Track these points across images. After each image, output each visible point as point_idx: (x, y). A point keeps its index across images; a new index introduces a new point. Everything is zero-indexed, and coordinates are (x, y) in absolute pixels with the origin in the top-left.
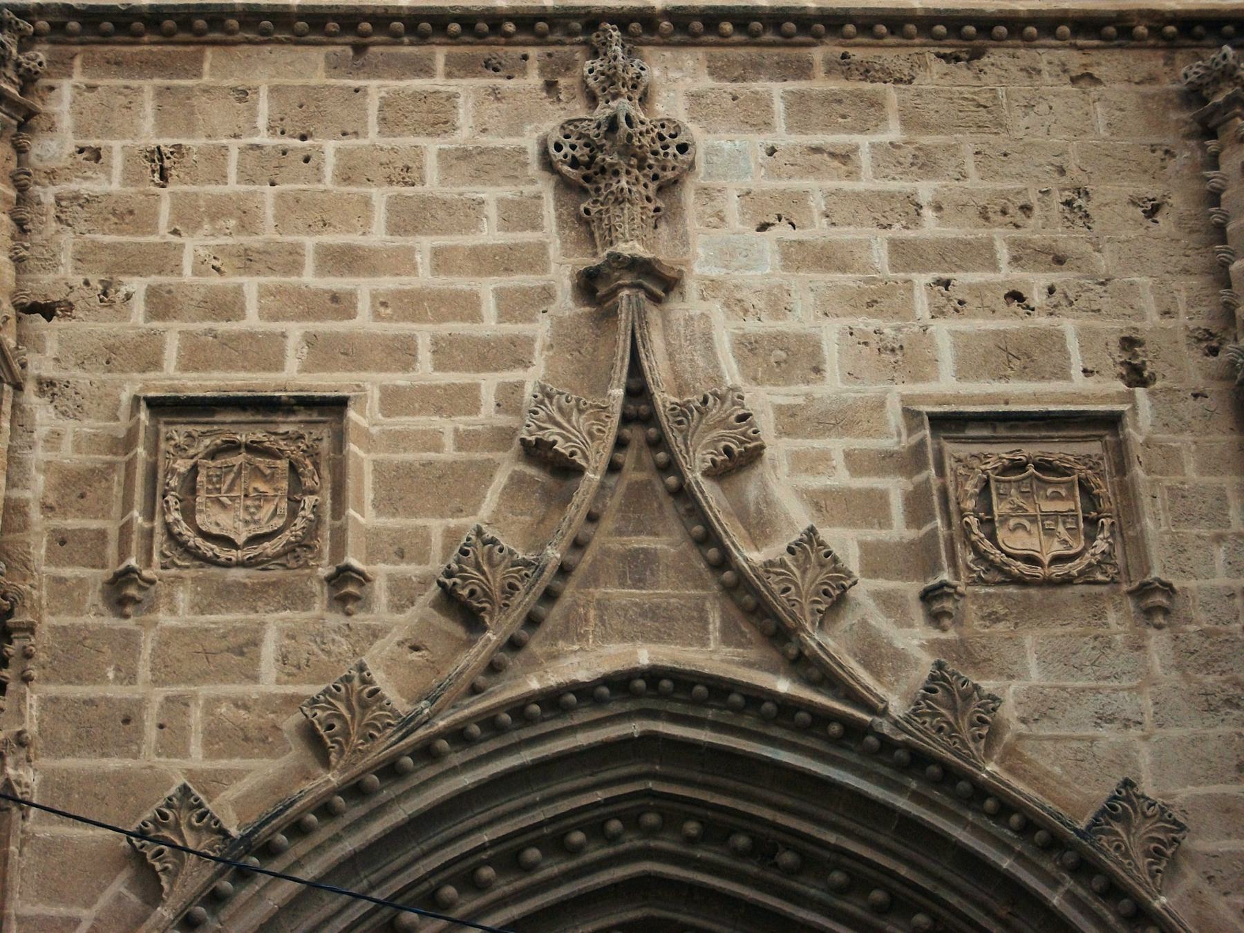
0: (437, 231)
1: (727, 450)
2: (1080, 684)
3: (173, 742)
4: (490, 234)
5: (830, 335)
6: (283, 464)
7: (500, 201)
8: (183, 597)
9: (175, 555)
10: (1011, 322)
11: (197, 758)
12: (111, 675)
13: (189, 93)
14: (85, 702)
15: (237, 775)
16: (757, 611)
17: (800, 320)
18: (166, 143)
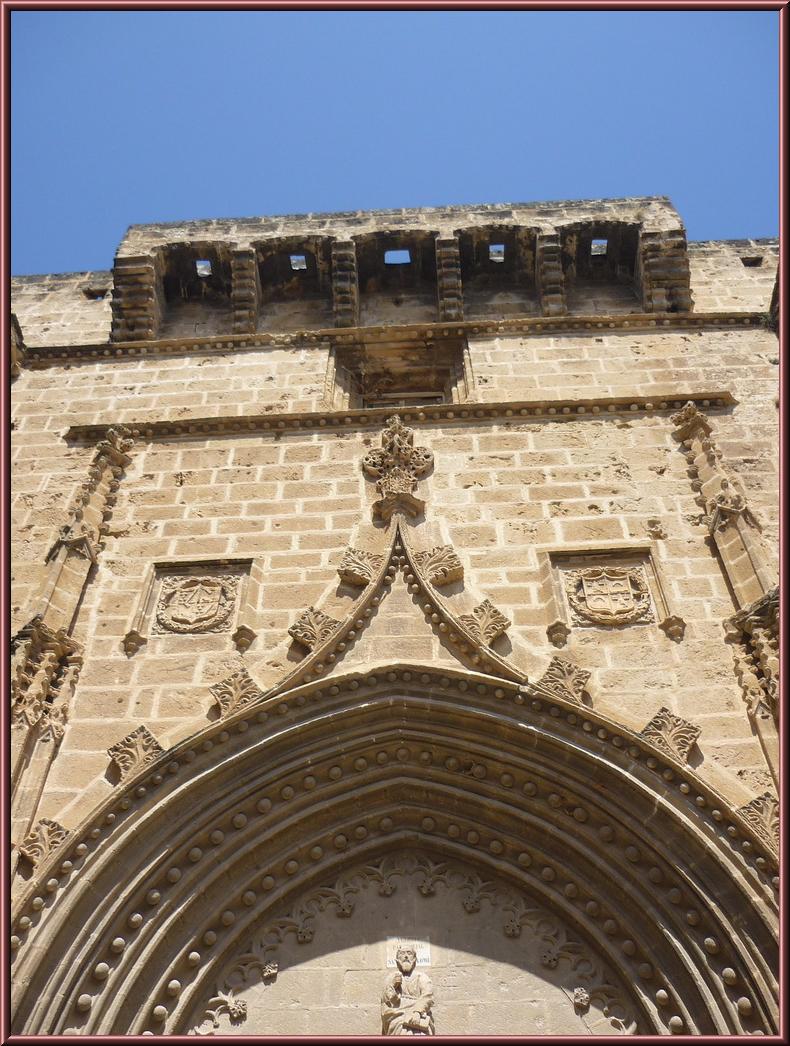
0: (304, 496)
1: (444, 570)
2: (636, 669)
3: (143, 706)
4: (333, 495)
5: (500, 528)
6: (219, 588)
7: (338, 483)
8: (160, 646)
9: (159, 628)
10: (592, 517)
11: (154, 717)
12: (117, 681)
13: (198, 453)
14: (101, 694)
15: (172, 725)
16: (454, 637)
17: (486, 518)
18: (184, 471)
